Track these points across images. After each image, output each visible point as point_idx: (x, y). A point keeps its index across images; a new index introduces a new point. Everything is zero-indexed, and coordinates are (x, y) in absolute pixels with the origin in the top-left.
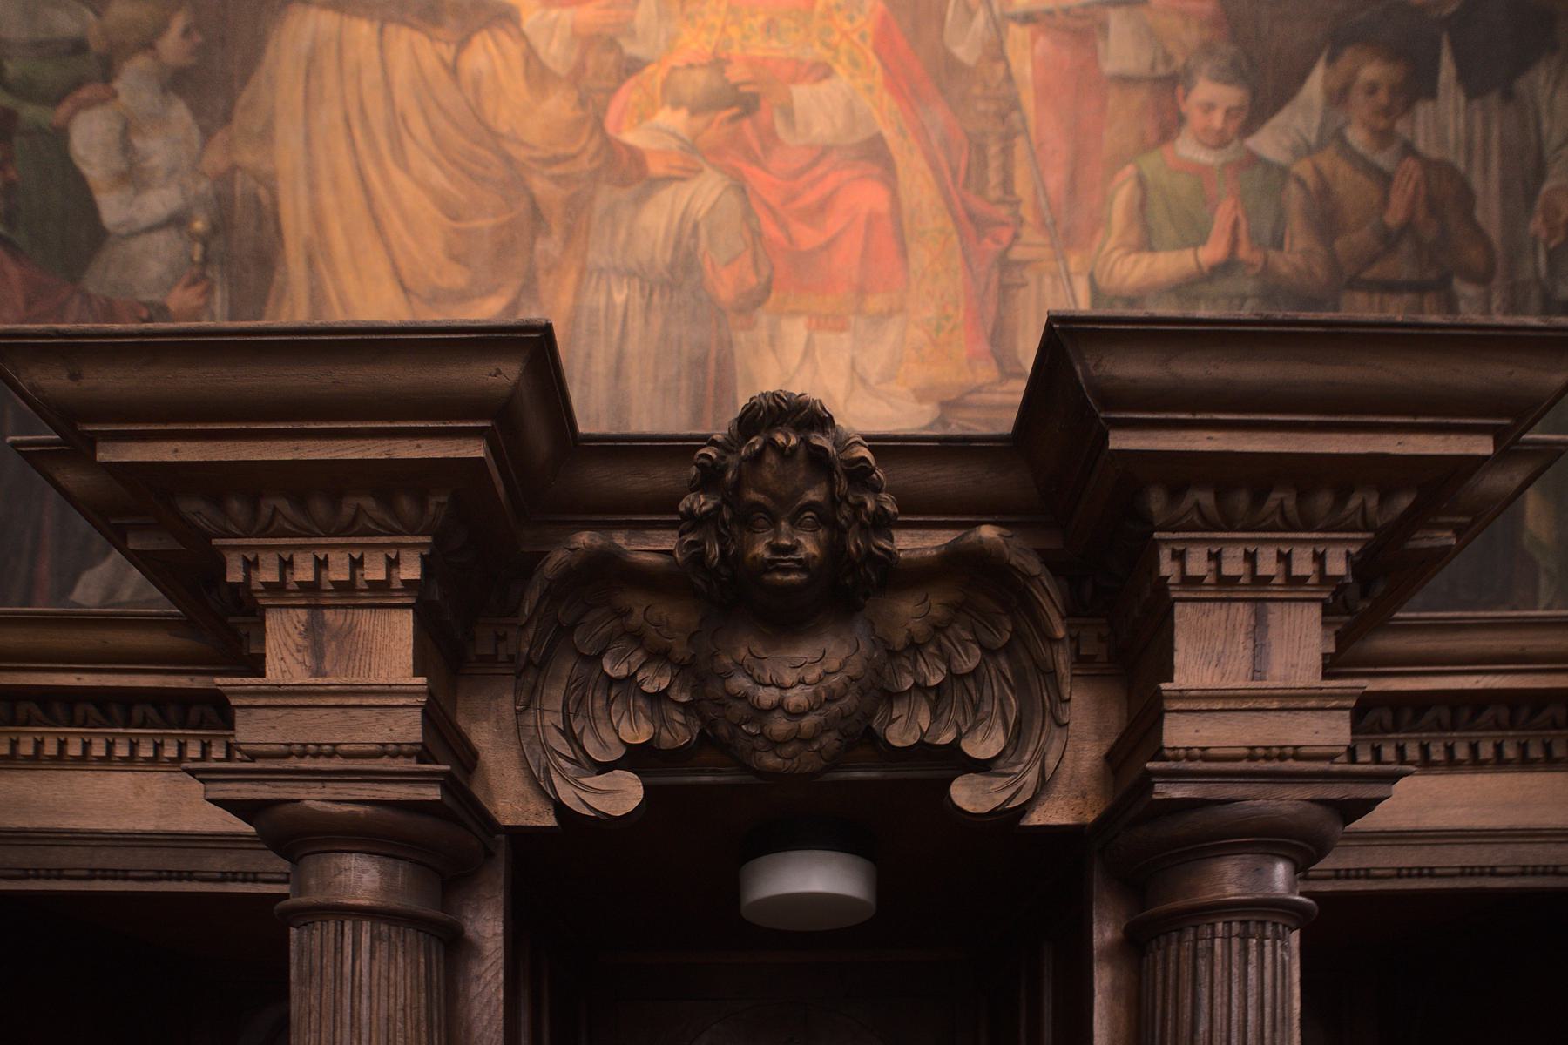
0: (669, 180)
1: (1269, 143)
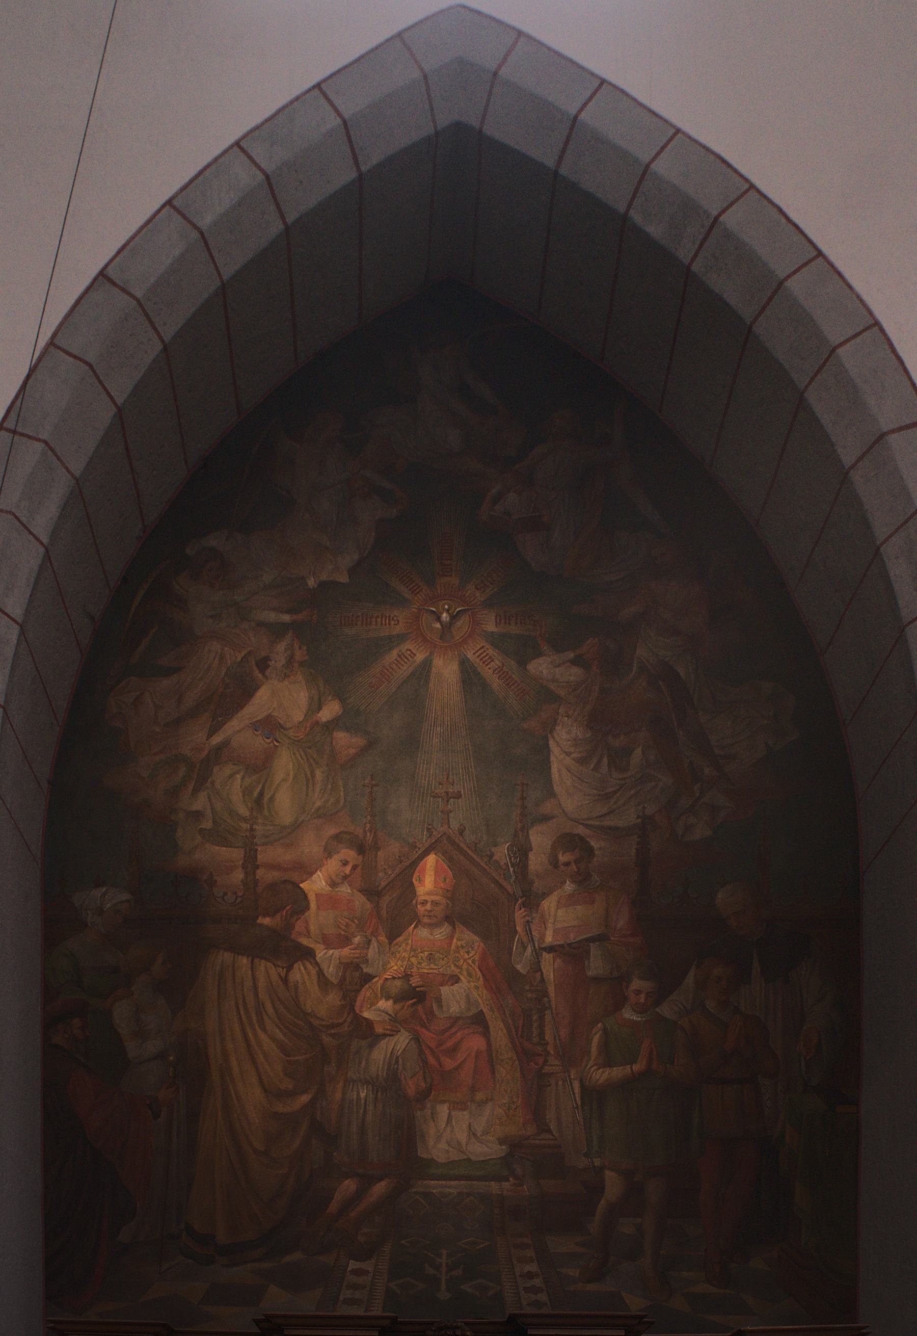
0: (385, 1036)
1: (666, 1010)
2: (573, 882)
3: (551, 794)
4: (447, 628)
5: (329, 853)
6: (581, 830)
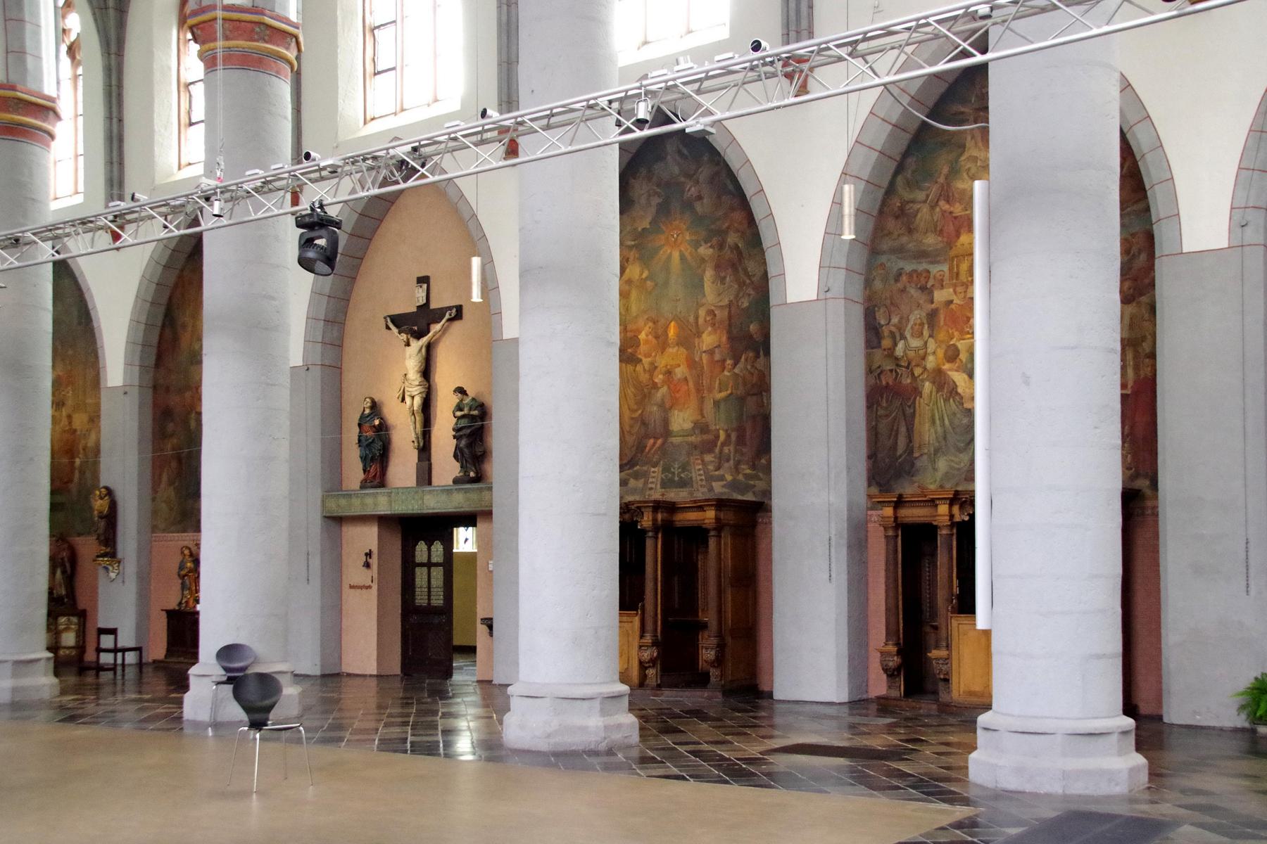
1: (736, 370)
4: (676, 240)
5: (645, 325)
6: (713, 308)
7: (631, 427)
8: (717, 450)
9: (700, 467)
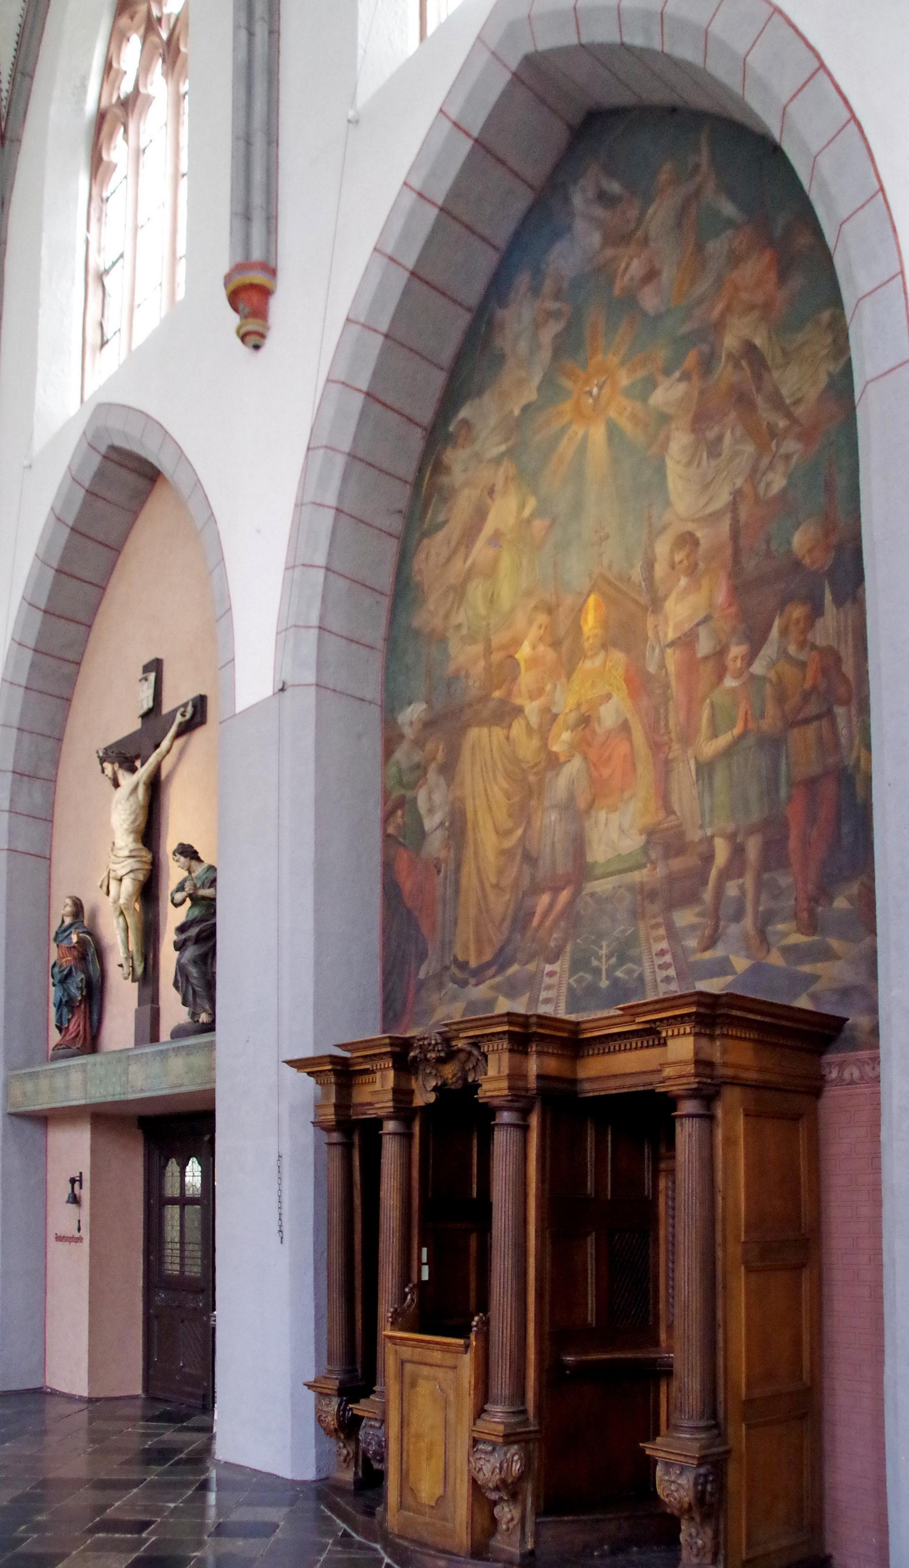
0: (565, 762)
1: (758, 668)
2: (686, 575)
3: (668, 503)
5: (530, 622)
6: (690, 527)
7: (500, 872)
8: (708, 895)
9: (664, 945)
